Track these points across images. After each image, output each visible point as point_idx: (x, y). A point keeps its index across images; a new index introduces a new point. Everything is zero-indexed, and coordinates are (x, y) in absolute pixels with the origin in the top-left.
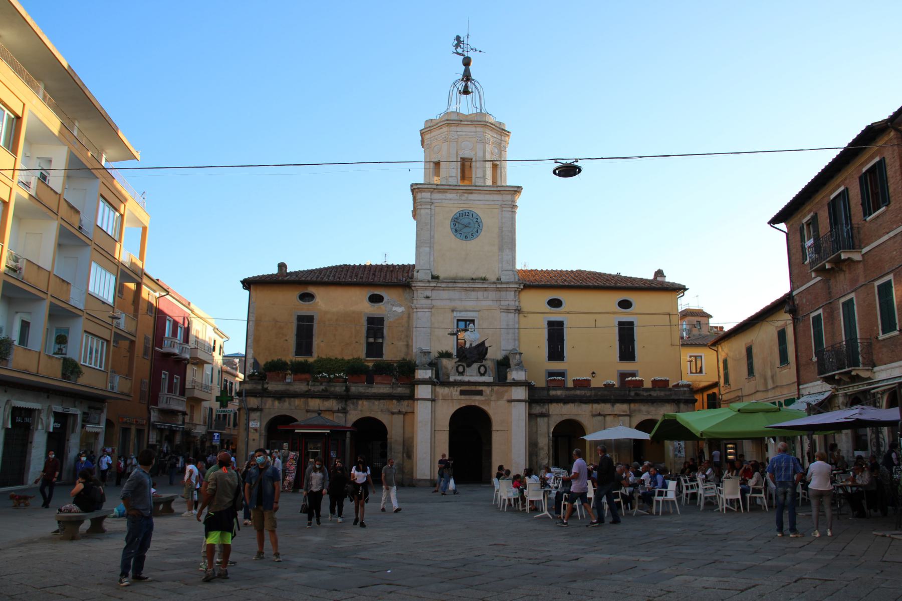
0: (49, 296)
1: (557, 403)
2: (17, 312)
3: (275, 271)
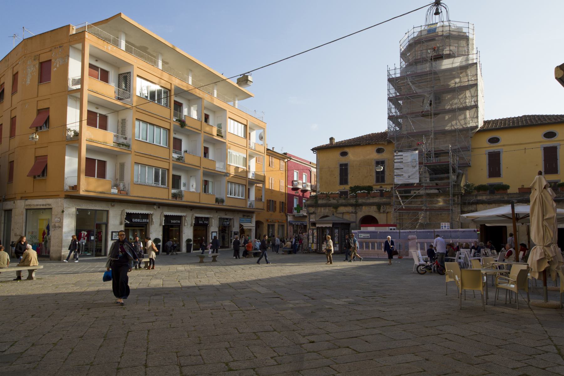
0: (202, 168)
1: (482, 204)
2: (191, 176)
3: (328, 142)
